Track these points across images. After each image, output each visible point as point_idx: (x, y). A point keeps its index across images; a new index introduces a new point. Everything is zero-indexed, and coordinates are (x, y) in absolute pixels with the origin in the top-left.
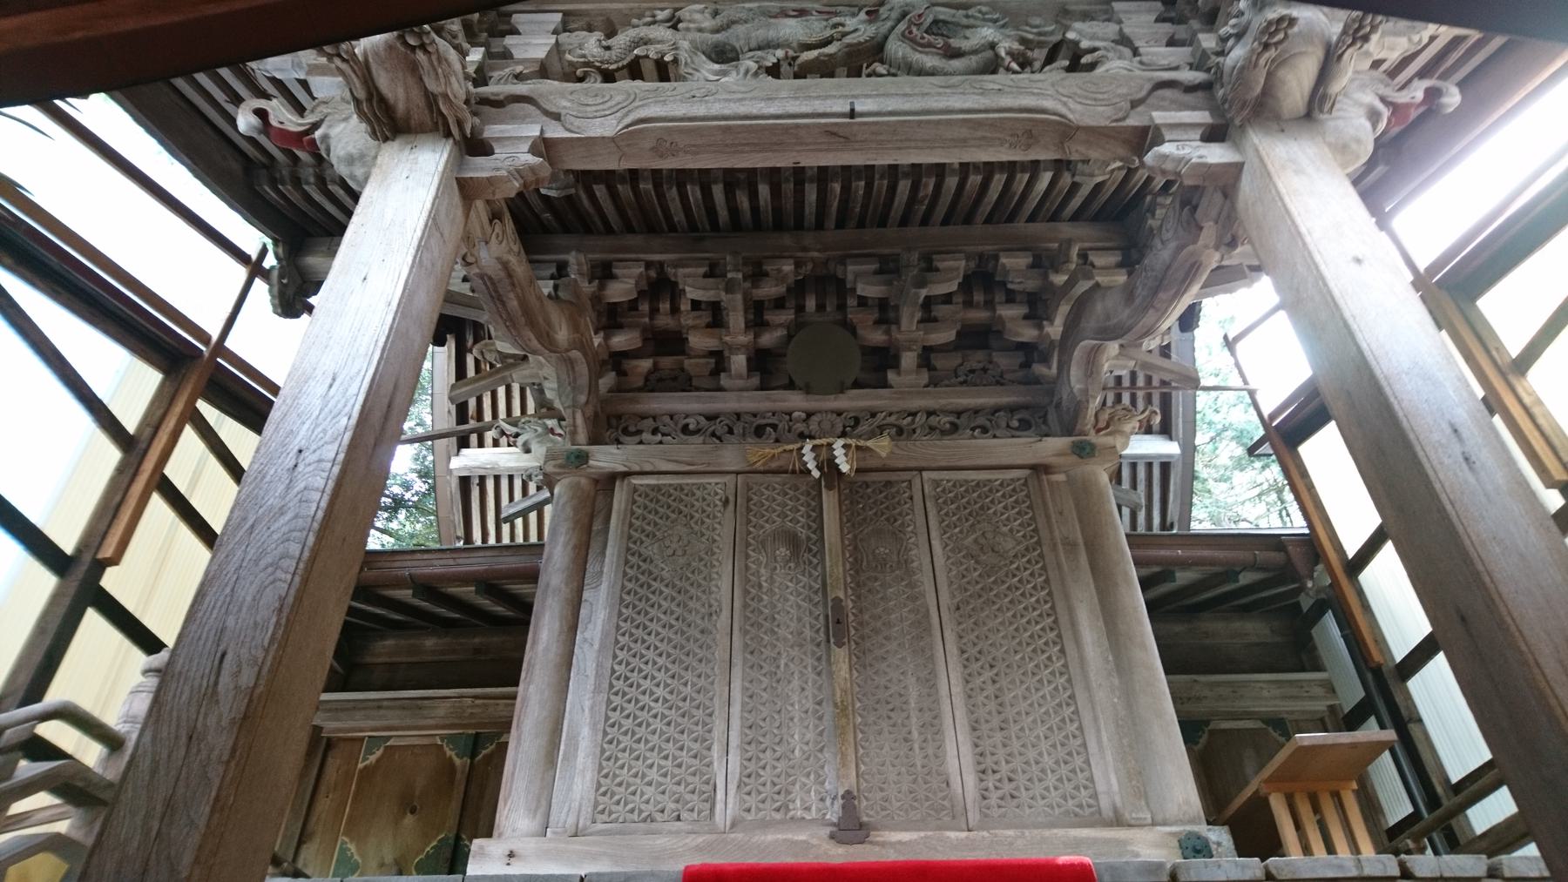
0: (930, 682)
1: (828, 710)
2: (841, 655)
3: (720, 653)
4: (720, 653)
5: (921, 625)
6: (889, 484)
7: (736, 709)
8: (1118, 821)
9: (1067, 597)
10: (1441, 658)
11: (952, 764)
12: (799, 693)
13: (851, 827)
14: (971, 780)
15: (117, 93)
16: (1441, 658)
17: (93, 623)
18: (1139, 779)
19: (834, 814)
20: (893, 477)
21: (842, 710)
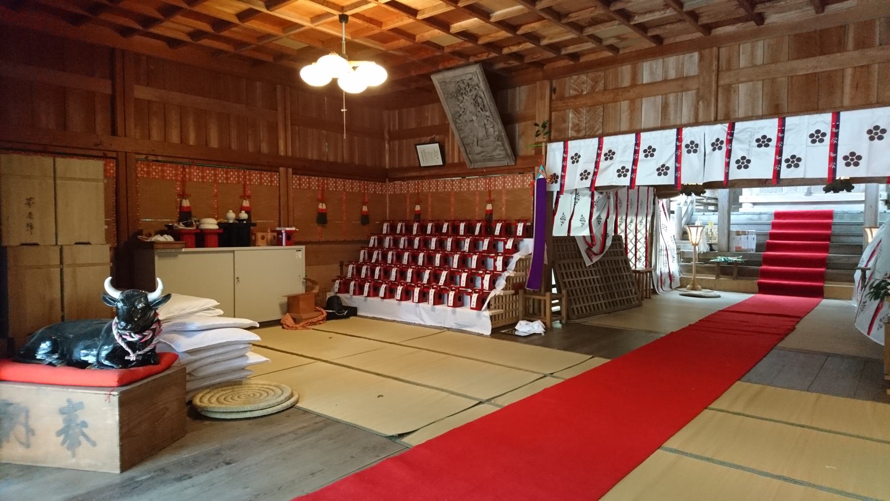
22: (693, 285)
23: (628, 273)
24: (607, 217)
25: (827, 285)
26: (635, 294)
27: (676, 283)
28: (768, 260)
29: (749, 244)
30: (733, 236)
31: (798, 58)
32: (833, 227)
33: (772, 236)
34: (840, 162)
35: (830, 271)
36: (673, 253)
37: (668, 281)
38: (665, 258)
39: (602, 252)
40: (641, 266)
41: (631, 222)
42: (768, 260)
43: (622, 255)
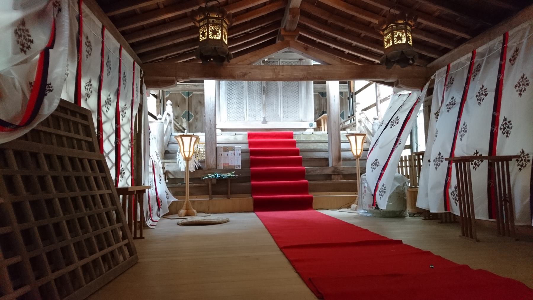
0: (277, 100)
1: (261, 105)
2: (264, 96)
3: (244, 95)
4: (244, 95)
5: (277, 90)
6: (274, 62)
7: (247, 104)
8: (302, 121)
9: (301, 86)
10: (459, 215)
11: (279, 113)
12: (257, 103)
13: (265, 122)
14: (282, 115)
15: (384, 239)
16: (459, 215)
17: (190, 138)
18: (306, 115)
19: (262, 119)
20: (275, 60)
21: (264, 105)
22: (187, 209)
23: (105, 192)
24: (51, 45)
25: (315, 196)
26: (124, 237)
27: (165, 209)
28: (255, 176)
29: (235, 161)
30: (220, 152)
31: (18, 263)
32: (297, 145)
33: (252, 153)
34: (395, 40)
35: (312, 182)
36: (160, 171)
37: (156, 208)
38: (152, 176)
39: (26, 123)
40: (125, 182)
41: (108, 102)
42: (255, 176)
43: (91, 148)
